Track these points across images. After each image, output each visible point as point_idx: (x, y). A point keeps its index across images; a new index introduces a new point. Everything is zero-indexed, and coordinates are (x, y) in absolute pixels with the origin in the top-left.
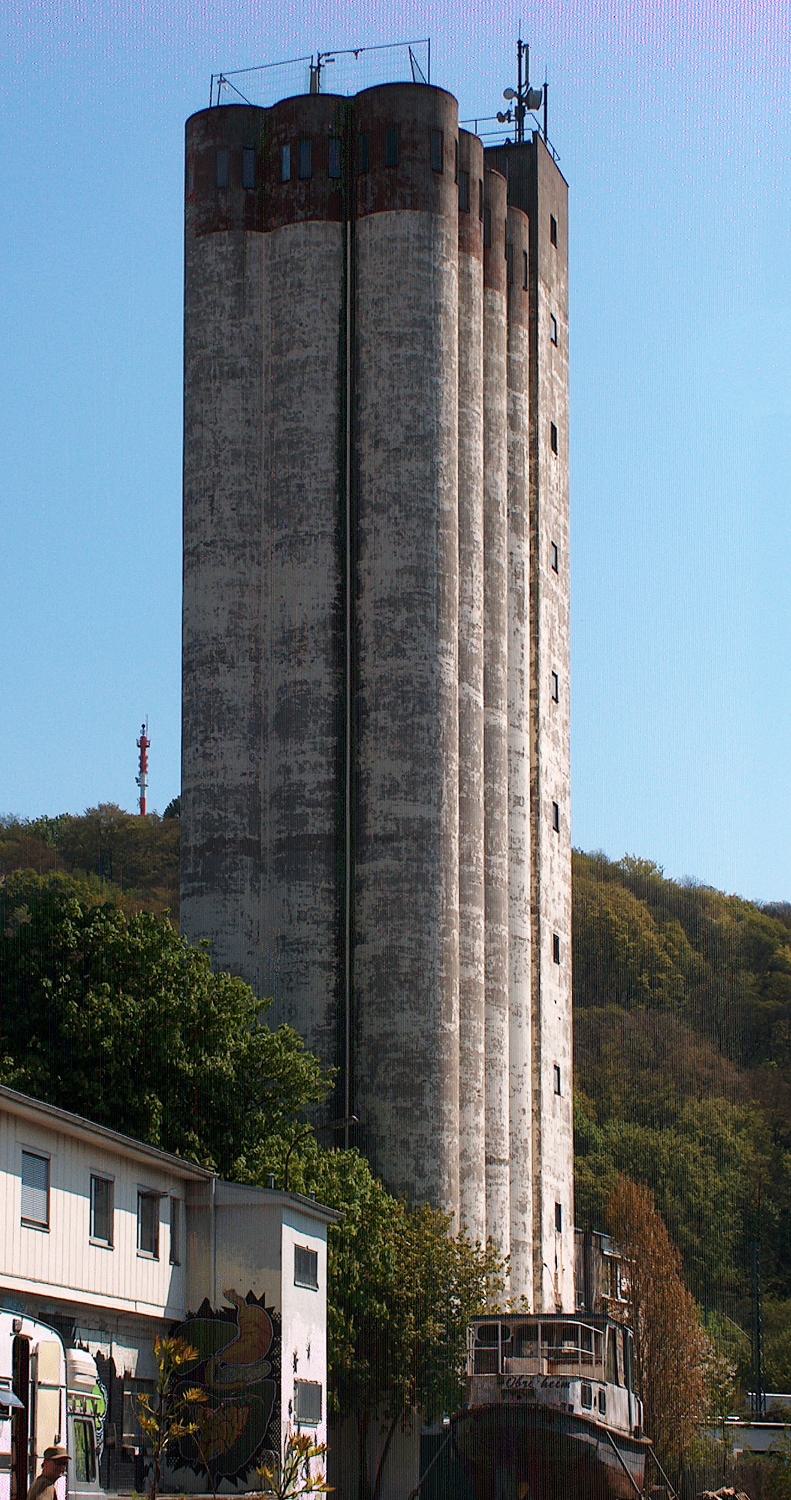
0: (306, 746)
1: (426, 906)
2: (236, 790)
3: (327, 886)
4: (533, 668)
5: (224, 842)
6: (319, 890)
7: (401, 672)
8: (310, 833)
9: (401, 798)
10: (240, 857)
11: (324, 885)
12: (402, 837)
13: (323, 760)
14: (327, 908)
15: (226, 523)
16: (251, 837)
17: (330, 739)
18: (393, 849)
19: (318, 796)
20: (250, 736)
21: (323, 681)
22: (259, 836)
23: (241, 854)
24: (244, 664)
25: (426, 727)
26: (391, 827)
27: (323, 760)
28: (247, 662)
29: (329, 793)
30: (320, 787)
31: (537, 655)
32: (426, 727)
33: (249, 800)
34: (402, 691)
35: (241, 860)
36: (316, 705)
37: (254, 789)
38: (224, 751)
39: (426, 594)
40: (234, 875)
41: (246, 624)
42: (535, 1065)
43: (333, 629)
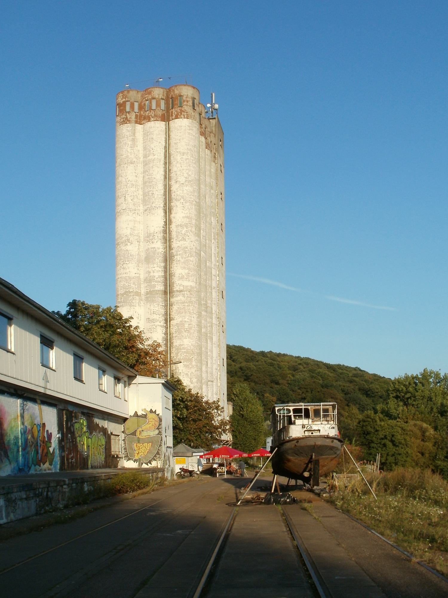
11: (161, 304)
13: (160, 269)
19: (159, 279)
20: (137, 263)
22: (141, 291)
26: (182, 288)
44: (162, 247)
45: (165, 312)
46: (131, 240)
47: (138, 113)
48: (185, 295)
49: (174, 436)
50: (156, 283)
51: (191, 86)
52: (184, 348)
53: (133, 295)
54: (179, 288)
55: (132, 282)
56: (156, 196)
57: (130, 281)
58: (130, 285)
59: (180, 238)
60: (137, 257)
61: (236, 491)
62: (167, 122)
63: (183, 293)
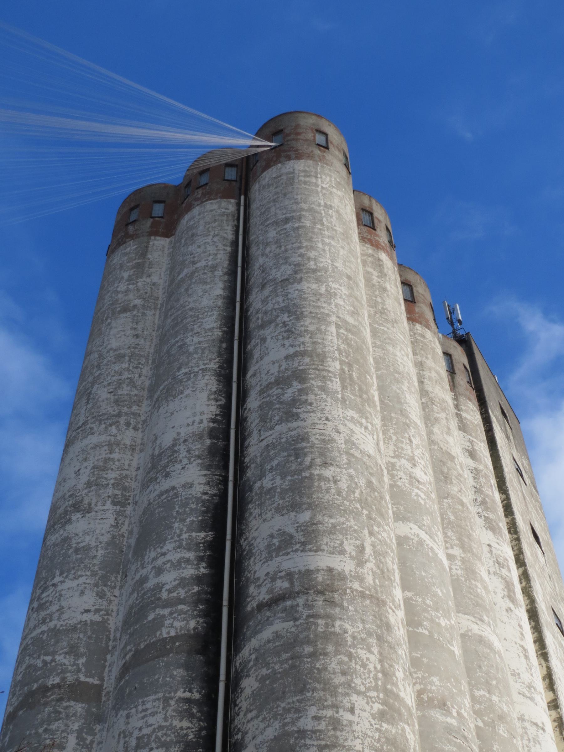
0: (169, 546)
1: (344, 673)
2: (74, 629)
3: (187, 695)
4: (547, 681)
5: (45, 689)
6: (172, 702)
7: (292, 433)
8: (165, 635)
9: (296, 551)
10: (65, 704)
11: (180, 694)
12: (298, 593)
13: (191, 555)
14: (185, 724)
15: (101, 404)
16: (88, 680)
17: (203, 534)
18: (284, 610)
19: (182, 592)
20: (100, 572)
21: (196, 483)
22: (102, 679)
23: (68, 701)
24: (105, 508)
25: (331, 478)
26: (282, 585)
27: (191, 555)
28: (109, 506)
29: (196, 589)
30: (183, 583)
31: (549, 668)
32: (331, 478)
33: (90, 638)
34: (295, 449)
35: (67, 707)
36: (185, 505)
37: (102, 626)
38: (63, 593)
39: (324, 370)
40: (53, 727)
41: (127, 733)
42: (521, 570)
43: (210, 439)
44: (203, 480)
45: (201, 729)
46: (86, 501)
47: (162, 217)
48: (300, 609)
49: (359, 233)
50: (166, 612)
51: (315, 115)
52: (387, 315)
53: (60, 700)
54: (270, 591)
55: (65, 644)
56: (191, 349)
57: (57, 642)
58: (53, 660)
59: (277, 418)
60: (101, 552)
61: (249, 743)
62: (242, 197)
63: (289, 603)
